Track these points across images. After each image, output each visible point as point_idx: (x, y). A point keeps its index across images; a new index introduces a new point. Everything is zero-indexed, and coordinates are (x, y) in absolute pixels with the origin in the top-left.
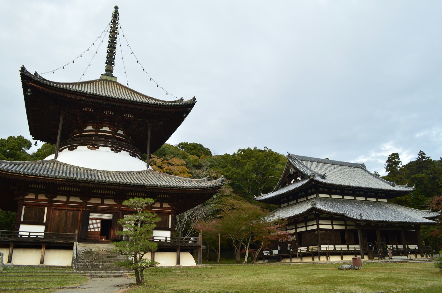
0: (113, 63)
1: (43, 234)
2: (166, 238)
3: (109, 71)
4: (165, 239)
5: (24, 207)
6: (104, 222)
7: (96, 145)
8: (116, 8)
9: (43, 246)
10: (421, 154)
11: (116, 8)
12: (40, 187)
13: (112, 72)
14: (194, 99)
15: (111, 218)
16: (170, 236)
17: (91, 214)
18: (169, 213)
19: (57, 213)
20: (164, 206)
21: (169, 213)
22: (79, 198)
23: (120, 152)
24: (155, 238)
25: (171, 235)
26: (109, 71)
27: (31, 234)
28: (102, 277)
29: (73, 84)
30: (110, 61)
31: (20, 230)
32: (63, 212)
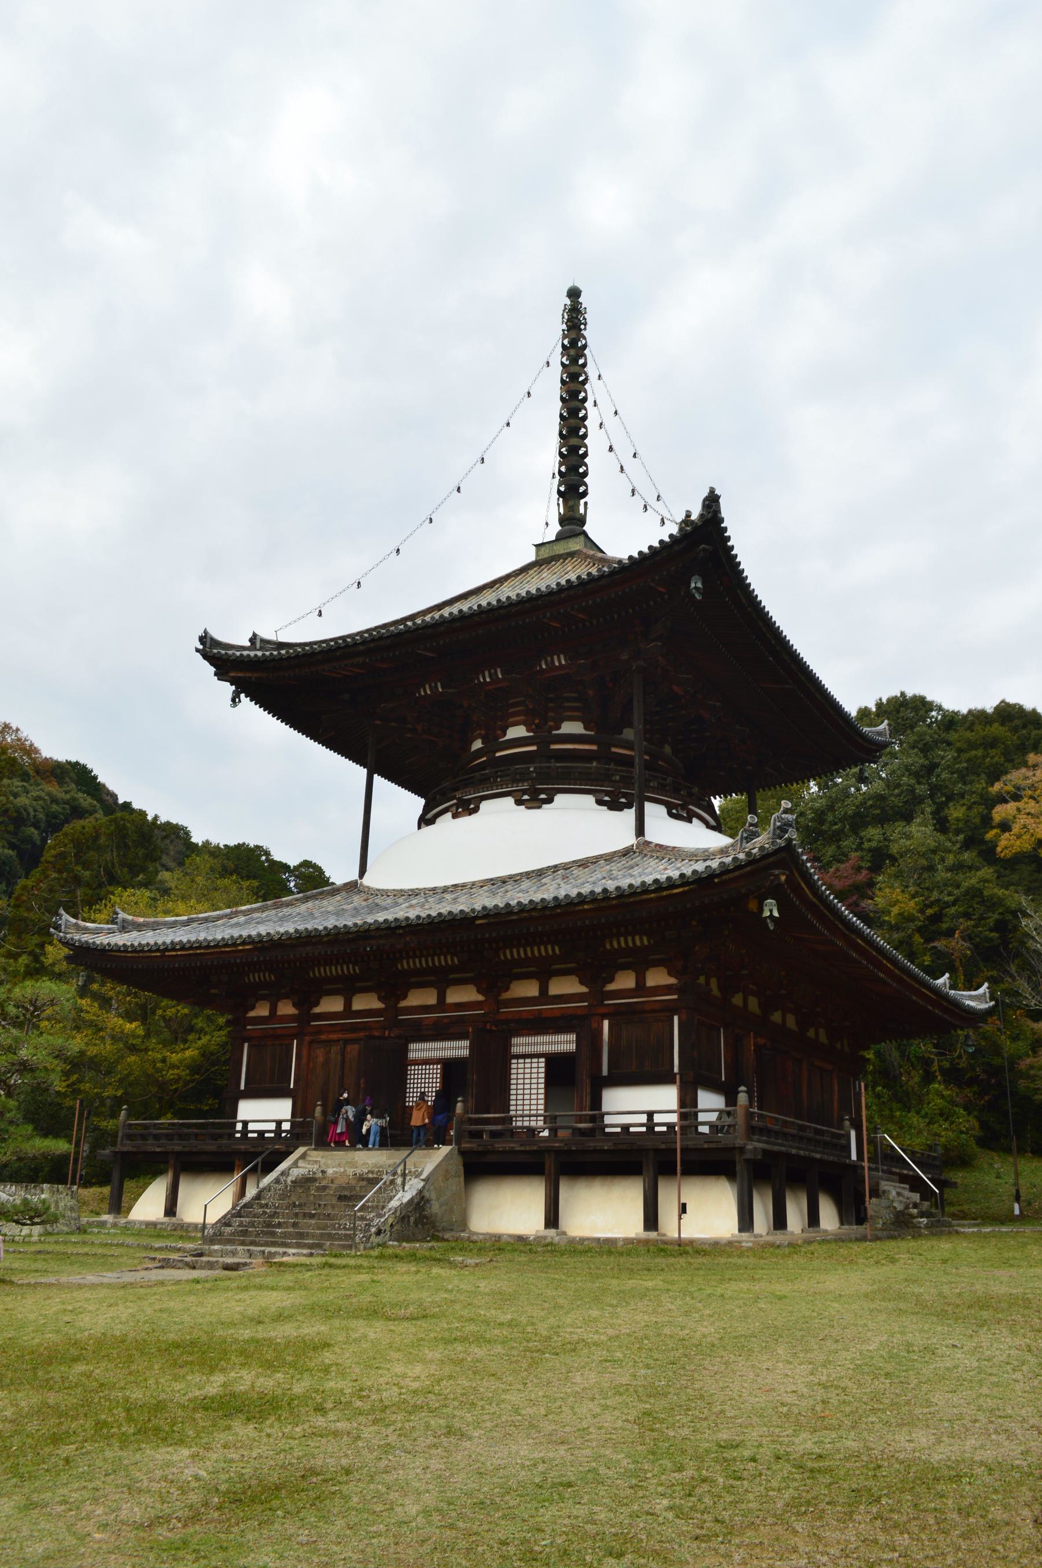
0: (582, 489)
2: (279, 1123)
3: (572, 522)
4: (272, 1126)
5: (246, 1045)
6: (450, 1067)
7: (543, 791)
8: (574, 294)
9: (237, 1162)
10: (205, 632)
11: (574, 294)
12: (638, 943)
14: (712, 501)
15: (572, 1047)
16: (289, 1117)
17: (412, 1046)
18: (670, 1009)
19: (320, 1054)
22: (665, 971)
23: (550, 801)
25: (293, 1114)
26: (572, 522)
27: (658, 1118)
28: (194, 1268)
31: (700, 1107)
32: (335, 1049)
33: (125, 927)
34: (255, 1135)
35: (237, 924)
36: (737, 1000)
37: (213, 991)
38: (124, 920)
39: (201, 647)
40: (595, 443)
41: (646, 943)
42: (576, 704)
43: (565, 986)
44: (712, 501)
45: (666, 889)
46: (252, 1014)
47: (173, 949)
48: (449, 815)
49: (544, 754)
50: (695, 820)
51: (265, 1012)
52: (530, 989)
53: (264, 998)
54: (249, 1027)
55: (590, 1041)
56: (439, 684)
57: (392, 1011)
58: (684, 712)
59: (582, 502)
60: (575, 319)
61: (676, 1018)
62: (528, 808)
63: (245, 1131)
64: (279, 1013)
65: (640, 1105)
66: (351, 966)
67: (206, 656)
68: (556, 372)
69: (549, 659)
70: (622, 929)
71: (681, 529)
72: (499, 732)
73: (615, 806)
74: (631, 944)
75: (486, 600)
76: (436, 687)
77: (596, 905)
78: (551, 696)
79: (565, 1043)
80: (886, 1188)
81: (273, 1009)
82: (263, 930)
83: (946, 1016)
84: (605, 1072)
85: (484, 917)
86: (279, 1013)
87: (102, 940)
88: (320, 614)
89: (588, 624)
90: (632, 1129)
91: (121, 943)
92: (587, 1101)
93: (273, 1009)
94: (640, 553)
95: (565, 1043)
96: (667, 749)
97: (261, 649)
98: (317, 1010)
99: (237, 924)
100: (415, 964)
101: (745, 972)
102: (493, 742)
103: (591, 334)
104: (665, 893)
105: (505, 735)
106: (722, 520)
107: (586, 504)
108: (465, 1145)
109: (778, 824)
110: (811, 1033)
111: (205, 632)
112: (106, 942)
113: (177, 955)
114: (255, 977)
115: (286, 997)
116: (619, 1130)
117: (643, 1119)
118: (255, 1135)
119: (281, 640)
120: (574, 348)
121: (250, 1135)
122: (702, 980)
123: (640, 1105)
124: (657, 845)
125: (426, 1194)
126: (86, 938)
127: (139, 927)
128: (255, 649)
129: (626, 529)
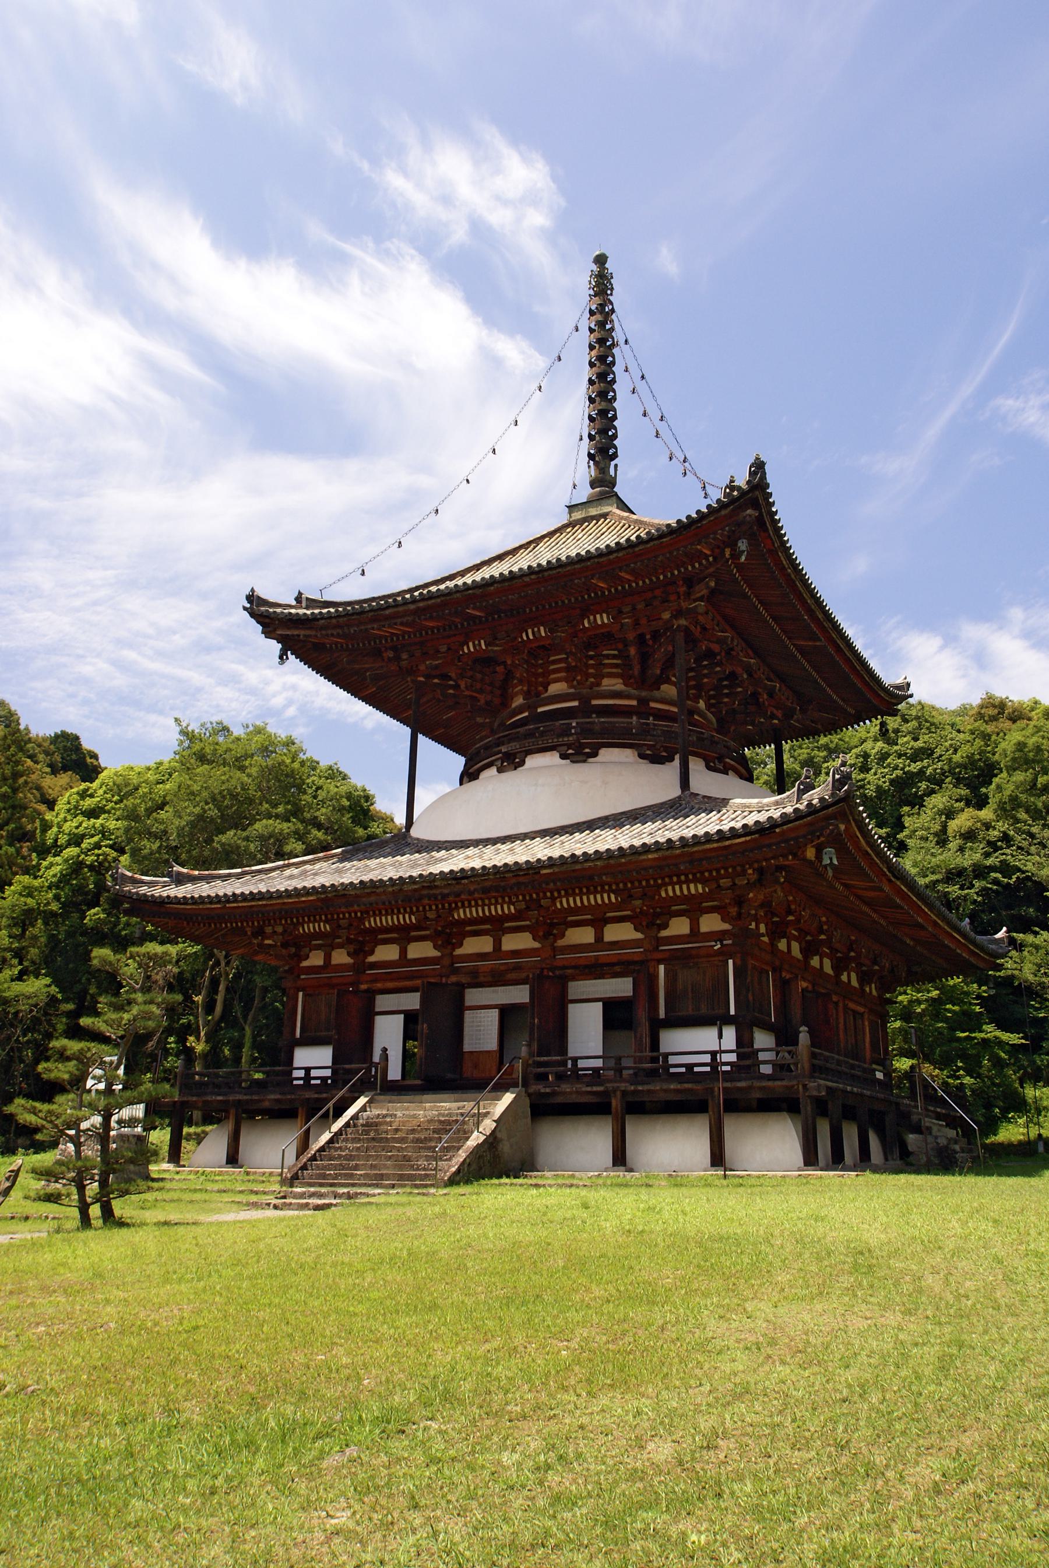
0: (611, 452)
1: (328, 1073)
3: (604, 485)
5: (301, 994)
6: (506, 1012)
8: (601, 260)
10: (253, 590)
11: (601, 260)
12: (693, 891)
13: (614, 485)
14: (758, 467)
15: (629, 993)
16: (330, 1064)
20: (411, 955)
21: (725, 954)
23: (595, 755)
24: (672, 1060)
26: (604, 485)
29: (462, 573)
30: (603, 448)
33: (180, 880)
34: (318, 1082)
35: (291, 877)
36: (782, 945)
37: (267, 942)
38: (179, 873)
39: (248, 605)
40: (624, 405)
41: (613, 900)
42: (615, 661)
43: (620, 932)
44: (758, 467)
45: (728, 839)
46: (305, 964)
47: (235, 901)
48: (493, 771)
49: (586, 709)
50: (730, 772)
51: (320, 962)
52: (584, 935)
53: (318, 947)
54: (303, 977)
55: (646, 984)
56: (482, 642)
57: (360, 967)
58: (718, 669)
59: (613, 463)
60: (602, 284)
61: (730, 962)
62: (573, 762)
63: (308, 1077)
64: (334, 962)
65: (696, 1045)
66: (407, 916)
67: (252, 615)
68: (584, 338)
69: (592, 617)
70: (683, 878)
71: (726, 495)
72: (541, 688)
73: (657, 758)
74: (686, 892)
75: (522, 562)
76: (480, 644)
77: (660, 854)
78: (591, 653)
79: (622, 987)
80: (927, 1124)
81: (328, 957)
82: (318, 882)
83: (972, 959)
84: (662, 1014)
85: (550, 866)
86: (334, 962)
87: (158, 892)
88: (363, 574)
89: (634, 585)
90: (696, 1069)
91: (180, 895)
92: (647, 1041)
93: (328, 957)
94: (688, 517)
95: (622, 987)
96: (702, 704)
97: (307, 608)
98: (371, 959)
99: (291, 877)
100: (471, 913)
101: (791, 918)
102: (534, 696)
103: (618, 298)
104: (727, 843)
105: (546, 691)
106: (768, 486)
107: (616, 466)
108: (533, 1088)
109: (837, 777)
110: (844, 978)
111: (253, 590)
112: (165, 894)
113: (238, 907)
114: (310, 928)
115: (341, 946)
116: (683, 1070)
117: (707, 1059)
118: (318, 1082)
119: (325, 598)
120: (602, 313)
121: (313, 1082)
122: (753, 926)
123: (696, 1045)
124: (704, 797)
125: (499, 1135)
126: (143, 890)
127: (193, 879)
128: (301, 607)
129: (662, 494)
